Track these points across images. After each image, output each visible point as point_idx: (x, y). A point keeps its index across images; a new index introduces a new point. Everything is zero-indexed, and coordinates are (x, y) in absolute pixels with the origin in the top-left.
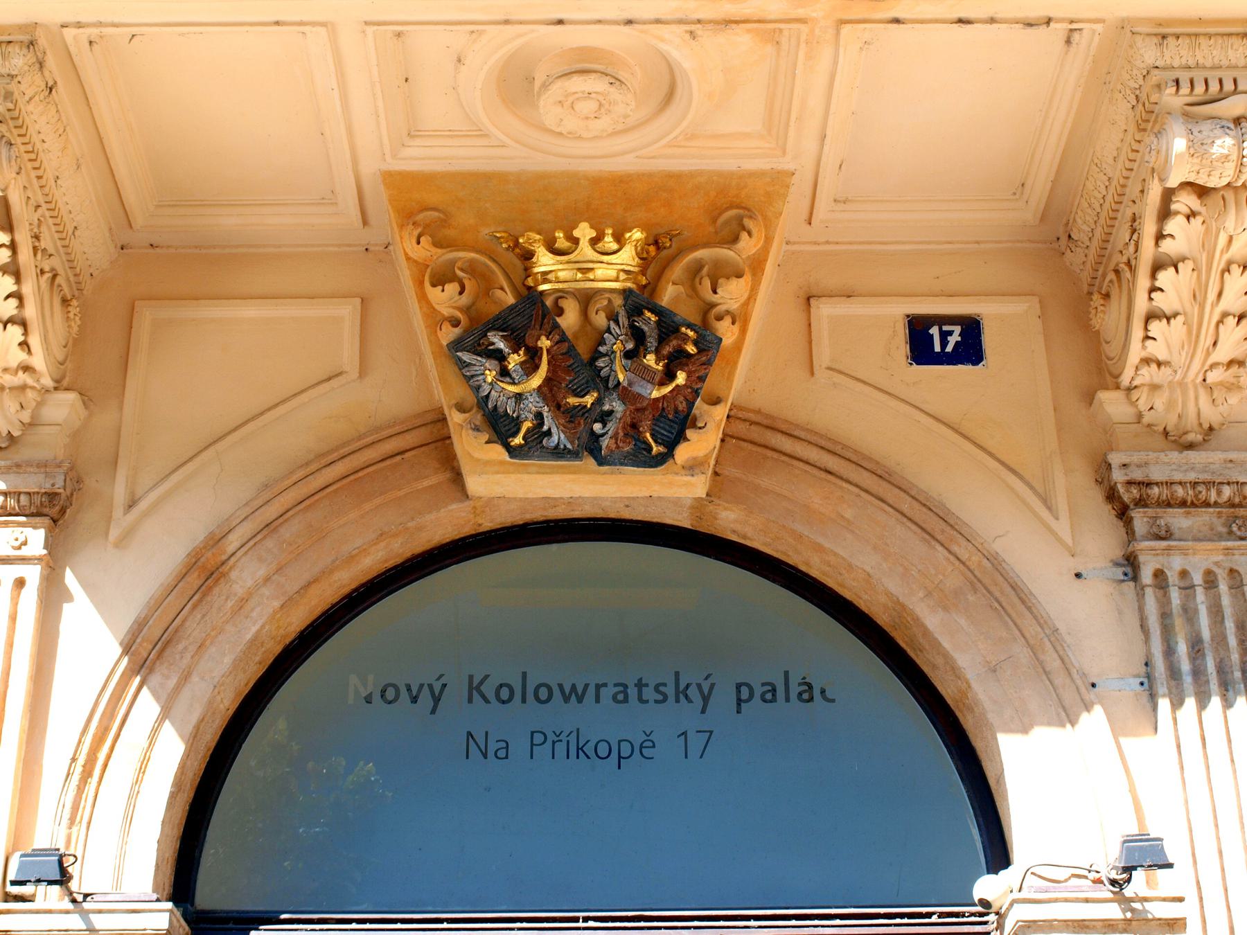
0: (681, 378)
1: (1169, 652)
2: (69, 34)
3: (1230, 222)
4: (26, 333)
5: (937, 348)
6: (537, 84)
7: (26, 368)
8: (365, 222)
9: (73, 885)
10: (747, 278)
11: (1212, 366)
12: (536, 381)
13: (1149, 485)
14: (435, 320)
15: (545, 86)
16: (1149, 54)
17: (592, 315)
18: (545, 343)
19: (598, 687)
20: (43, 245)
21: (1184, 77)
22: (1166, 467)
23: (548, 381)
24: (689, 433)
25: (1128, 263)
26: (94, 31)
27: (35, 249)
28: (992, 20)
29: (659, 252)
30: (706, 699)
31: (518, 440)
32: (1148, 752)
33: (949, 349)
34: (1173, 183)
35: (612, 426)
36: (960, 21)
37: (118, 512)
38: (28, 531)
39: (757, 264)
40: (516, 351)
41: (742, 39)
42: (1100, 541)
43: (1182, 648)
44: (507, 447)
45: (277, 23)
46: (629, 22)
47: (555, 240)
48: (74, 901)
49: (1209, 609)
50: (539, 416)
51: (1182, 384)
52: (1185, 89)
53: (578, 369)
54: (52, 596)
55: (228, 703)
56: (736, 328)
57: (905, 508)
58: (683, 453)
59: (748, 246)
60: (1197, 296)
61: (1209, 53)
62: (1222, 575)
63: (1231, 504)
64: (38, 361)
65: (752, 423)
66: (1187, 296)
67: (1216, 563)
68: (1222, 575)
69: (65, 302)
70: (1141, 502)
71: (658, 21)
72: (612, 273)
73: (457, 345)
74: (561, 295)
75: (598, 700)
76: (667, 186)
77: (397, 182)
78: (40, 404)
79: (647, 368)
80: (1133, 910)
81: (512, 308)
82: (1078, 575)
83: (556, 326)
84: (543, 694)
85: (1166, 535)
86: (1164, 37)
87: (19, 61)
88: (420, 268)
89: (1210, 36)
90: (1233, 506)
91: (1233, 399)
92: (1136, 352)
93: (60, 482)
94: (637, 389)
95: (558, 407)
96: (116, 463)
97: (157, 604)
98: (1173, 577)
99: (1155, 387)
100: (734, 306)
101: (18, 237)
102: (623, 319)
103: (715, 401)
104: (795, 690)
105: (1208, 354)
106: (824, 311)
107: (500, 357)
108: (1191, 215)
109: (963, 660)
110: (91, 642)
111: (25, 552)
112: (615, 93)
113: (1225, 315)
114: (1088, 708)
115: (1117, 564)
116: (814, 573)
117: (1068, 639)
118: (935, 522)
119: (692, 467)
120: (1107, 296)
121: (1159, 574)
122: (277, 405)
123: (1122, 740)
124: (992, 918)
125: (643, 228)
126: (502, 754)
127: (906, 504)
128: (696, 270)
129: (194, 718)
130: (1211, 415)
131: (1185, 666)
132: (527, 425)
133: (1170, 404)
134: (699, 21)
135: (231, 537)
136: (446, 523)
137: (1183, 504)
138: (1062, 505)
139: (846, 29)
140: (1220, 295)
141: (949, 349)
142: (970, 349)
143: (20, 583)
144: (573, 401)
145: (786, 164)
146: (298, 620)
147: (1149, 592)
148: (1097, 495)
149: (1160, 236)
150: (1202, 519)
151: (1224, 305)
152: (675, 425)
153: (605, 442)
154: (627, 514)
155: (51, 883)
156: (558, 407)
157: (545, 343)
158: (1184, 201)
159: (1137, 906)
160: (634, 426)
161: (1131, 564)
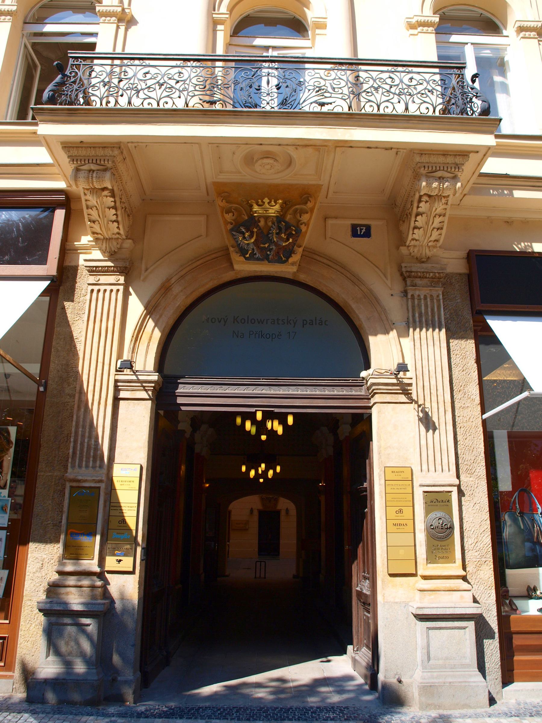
0: (291, 240)
1: (414, 316)
2: (129, 145)
3: (436, 205)
4: (118, 225)
5: (359, 233)
6: (255, 160)
7: (119, 234)
8: (208, 194)
9: (134, 369)
10: (309, 213)
11: (430, 241)
12: (253, 240)
13: (412, 272)
14: (226, 223)
15: (257, 161)
16: (417, 159)
17: (268, 223)
18: (255, 230)
19: (267, 320)
20: (123, 201)
21: (426, 165)
22: (416, 267)
23: (255, 240)
24: (293, 255)
25: (410, 213)
26: (136, 144)
27: (121, 202)
28: (377, 148)
29: (285, 208)
30: (295, 324)
31: (248, 256)
32: (406, 342)
33: (362, 233)
34: (422, 193)
35: (272, 253)
36: (368, 148)
37: (143, 272)
38: (120, 277)
39: (312, 210)
40: (247, 232)
41: (310, 150)
42: (398, 287)
43: (417, 315)
44: (245, 257)
45: (185, 143)
46: (280, 145)
47: (258, 202)
48: (134, 372)
49: (425, 305)
50: (253, 249)
51: (422, 246)
52: (426, 169)
53: (264, 237)
54: (126, 295)
55: (171, 322)
56: (306, 227)
57: (348, 276)
58: (291, 260)
59: (310, 205)
60: (427, 223)
61: (433, 159)
62: (428, 296)
63: (432, 278)
64: (122, 232)
65: (309, 252)
66: (424, 223)
67: (427, 293)
68: (428, 296)
69: (128, 216)
70: (409, 277)
71: (287, 145)
72: (273, 211)
73: (232, 230)
74: (259, 217)
75: (267, 323)
76: (289, 187)
77: (216, 185)
78: (122, 243)
79: (282, 237)
80: (400, 381)
81: (246, 220)
82: (392, 295)
83: (258, 225)
84: (253, 321)
85: (415, 285)
86: (422, 154)
87: (116, 152)
88: (222, 208)
89: (434, 154)
90: (433, 278)
91: (435, 250)
92: (410, 237)
93: (128, 264)
94: (279, 243)
95: (258, 247)
96: (142, 258)
97: (153, 297)
98: (416, 296)
99: (415, 246)
100: (305, 221)
101: (116, 199)
102: (276, 224)
103: (300, 247)
104: (318, 322)
105: (429, 238)
106: (330, 222)
107: (243, 234)
108: (426, 202)
109: (361, 316)
110: (136, 307)
111: (119, 282)
112: (275, 163)
113: (434, 228)
114: (392, 330)
115: (402, 292)
116: (324, 292)
117: (388, 312)
118: (356, 280)
119: (293, 264)
120: (404, 221)
121: (412, 295)
122: (184, 244)
123: (401, 339)
124: (365, 381)
125: (281, 199)
126: (242, 336)
127: (349, 275)
128: (296, 211)
129: (163, 326)
130: (429, 254)
131: (417, 320)
132: (250, 252)
133: (419, 251)
134: (298, 145)
135: (173, 279)
136: (228, 276)
137: (420, 277)
138: (389, 277)
139: (338, 149)
140: (433, 223)
141: (362, 233)
142: (367, 234)
143: (118, 290)
144: (262, 246)
145: (320, 183)
146: (189, 301)
147: (410, 300)
148: (398, 274)
149: (418, 207)
150: (425, 281)
151: (434, 226)
152: (289, 252)
153: (270, 257)
154: (276, 275)
155: (128, 368)
156: (258, 247)
157: (255, 230)
158: (425, 198)
159: (401, 380)
160: (278, 253)
161: (405, 293)
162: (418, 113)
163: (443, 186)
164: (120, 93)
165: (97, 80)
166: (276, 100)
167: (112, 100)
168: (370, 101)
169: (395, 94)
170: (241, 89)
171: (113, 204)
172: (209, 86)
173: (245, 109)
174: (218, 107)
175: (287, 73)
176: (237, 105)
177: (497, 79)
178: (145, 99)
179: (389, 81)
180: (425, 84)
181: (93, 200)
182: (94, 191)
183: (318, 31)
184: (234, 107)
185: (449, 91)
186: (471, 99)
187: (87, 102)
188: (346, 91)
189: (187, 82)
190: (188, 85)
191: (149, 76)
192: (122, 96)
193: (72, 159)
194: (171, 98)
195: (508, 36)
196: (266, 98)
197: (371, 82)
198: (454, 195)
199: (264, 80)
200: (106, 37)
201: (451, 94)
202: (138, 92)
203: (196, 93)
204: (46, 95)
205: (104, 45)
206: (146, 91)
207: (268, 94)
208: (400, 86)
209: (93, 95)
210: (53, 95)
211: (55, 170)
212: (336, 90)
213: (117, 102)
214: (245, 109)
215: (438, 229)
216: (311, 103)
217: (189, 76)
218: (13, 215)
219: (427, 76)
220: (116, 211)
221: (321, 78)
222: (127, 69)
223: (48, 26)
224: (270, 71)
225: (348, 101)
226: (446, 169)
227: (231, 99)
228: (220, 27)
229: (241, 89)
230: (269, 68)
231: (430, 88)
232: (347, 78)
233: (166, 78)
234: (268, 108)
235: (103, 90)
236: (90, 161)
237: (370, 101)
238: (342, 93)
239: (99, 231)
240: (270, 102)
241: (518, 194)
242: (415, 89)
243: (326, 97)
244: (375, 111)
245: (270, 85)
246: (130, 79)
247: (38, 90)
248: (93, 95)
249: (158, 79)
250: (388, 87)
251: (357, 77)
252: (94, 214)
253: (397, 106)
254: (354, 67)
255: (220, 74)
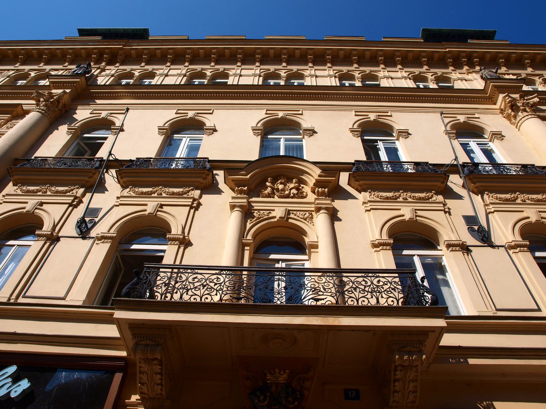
12: (266, 403)
18: (268, 394)
34: (397, 364)
92: (391, 400)
108: (401, 371)
113: (410, 392)
149: (395, 375)
151: (409, 390)
157: (268, 394)
158: (399, 368)
162: (386, 304)
163: (412, 358)
164: (175, 291)
165: (162, 282)
166: (284, 297)
167: (169, 295)
168: (351, 297)
169: (368, 292)
170: (260, 290)
171: (160, 370)
172: (237, 287)
173: (262, 304)
174: (243, 302)
175: (292, 279)
176: (257, 301)
177: (440, 277)
178: (192, 296)
179: (363, 283)
180: (389, 284)
181: (145, 367)
182: (148, 361)
183: (312, 250)
184: (254, 302)
185: (406, 289)
186: (423, 293)
187: (152, 296)
188: (333, 290)
189: (223, 284)
190: (223, 286)
191: (196, 280)
192: (176, 293)
193: (134, 336)
194: (211, 295)
195: (441, 250)
196: (277, 296)
197: (351, 284)
198: (422, 365)
199: (276, 283)
200: (170, 253)
201: (408, 290)
202: (188, 290)
203: (228, 292)
204: (124, 290)
205: (168, 260)
206: (193, 290)
207: (279, 293)
208: (372, 286)
209: (157, 292)
210: (129, 291)
211: (121, 342)
212: (327, 290)
213: (172, 297)
214: (262, 304)
215: (413, 392)
216: (309, 299)
217: (224, 280)
218: (83, 375)
219: (390, 279)
220: (162, 376)
221: (316, 282)
222: (182, 275)
223: (134, 245)
224: (280, 277)
225: (335, 297)
226: (412, 345)
227: (252, 296)
228: (246, 248)
229: (260, 290)
230: (279, 275)
231: (393, 287)
232: (334, 282)
233: (208, 282)
234: (279, 302)
235: (164, 289)
236: (148, 338)
237: (351, 297)
238: (330, 292)
239: (146, 391)
240: (280, 299)
241: (471, 361)
242: (383, 288)
243: (320, 295)
244: (355, 304)
245: (280, 287)
246: (183, 282)
247: (120, 284)
248: (157, 292)
249: (202, 282)
250: (363, 287)
251: (342, 284)
252: (144, 378)
253: (370, 300)
254: (338, 274)
255: (245, 279)
